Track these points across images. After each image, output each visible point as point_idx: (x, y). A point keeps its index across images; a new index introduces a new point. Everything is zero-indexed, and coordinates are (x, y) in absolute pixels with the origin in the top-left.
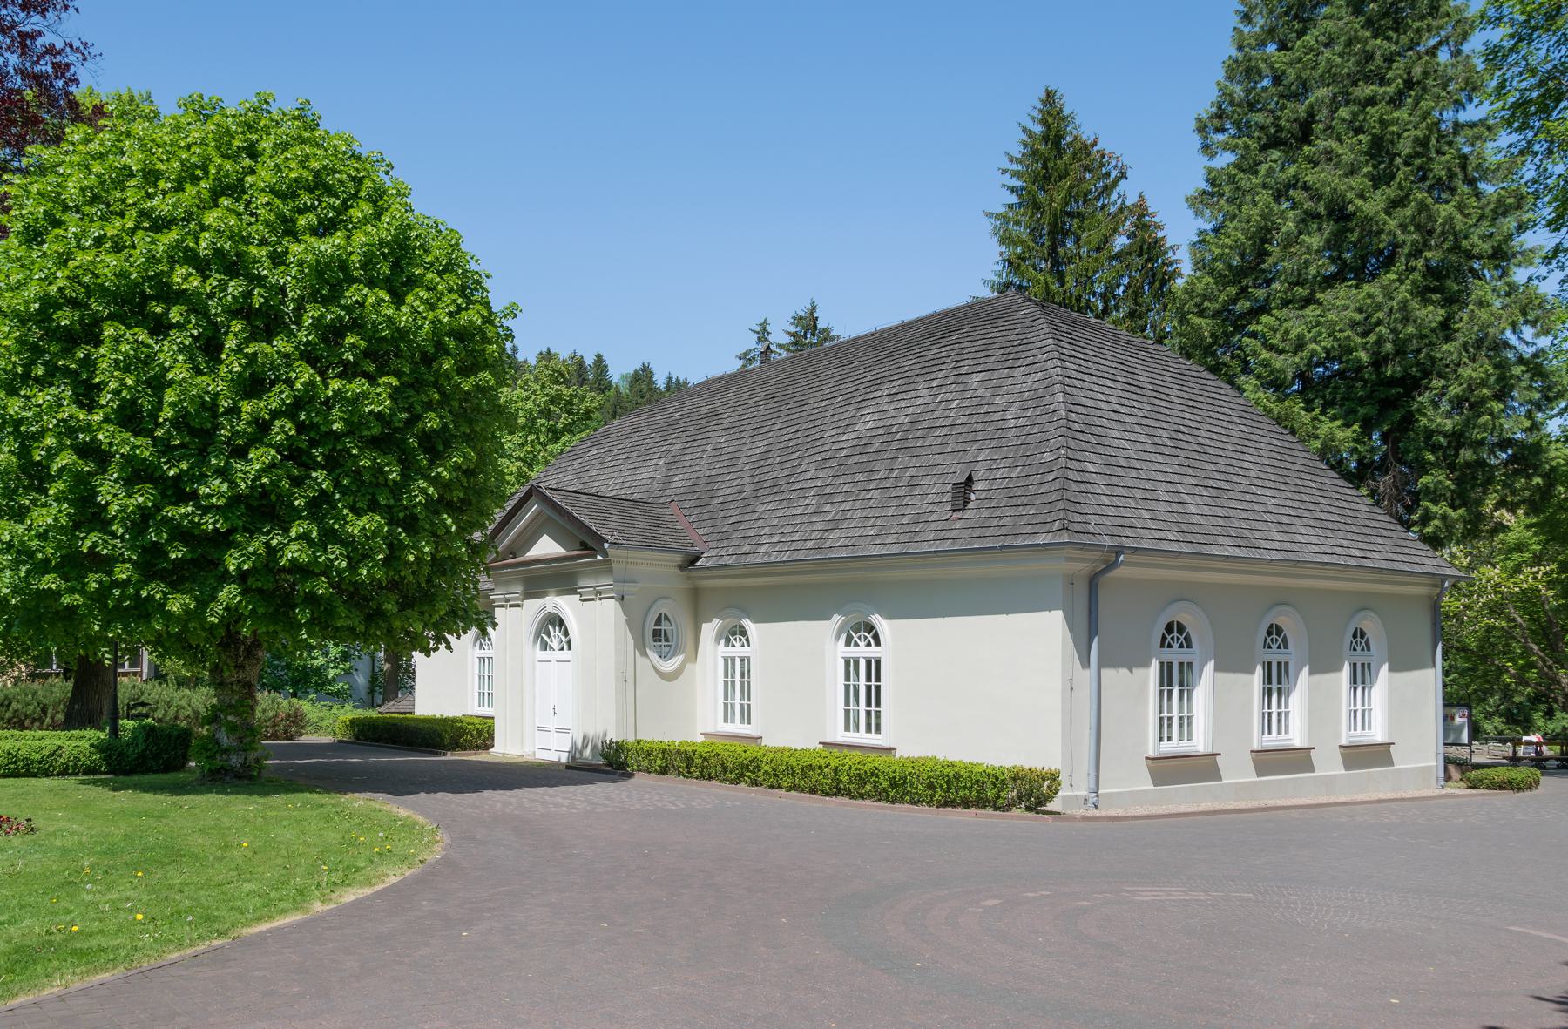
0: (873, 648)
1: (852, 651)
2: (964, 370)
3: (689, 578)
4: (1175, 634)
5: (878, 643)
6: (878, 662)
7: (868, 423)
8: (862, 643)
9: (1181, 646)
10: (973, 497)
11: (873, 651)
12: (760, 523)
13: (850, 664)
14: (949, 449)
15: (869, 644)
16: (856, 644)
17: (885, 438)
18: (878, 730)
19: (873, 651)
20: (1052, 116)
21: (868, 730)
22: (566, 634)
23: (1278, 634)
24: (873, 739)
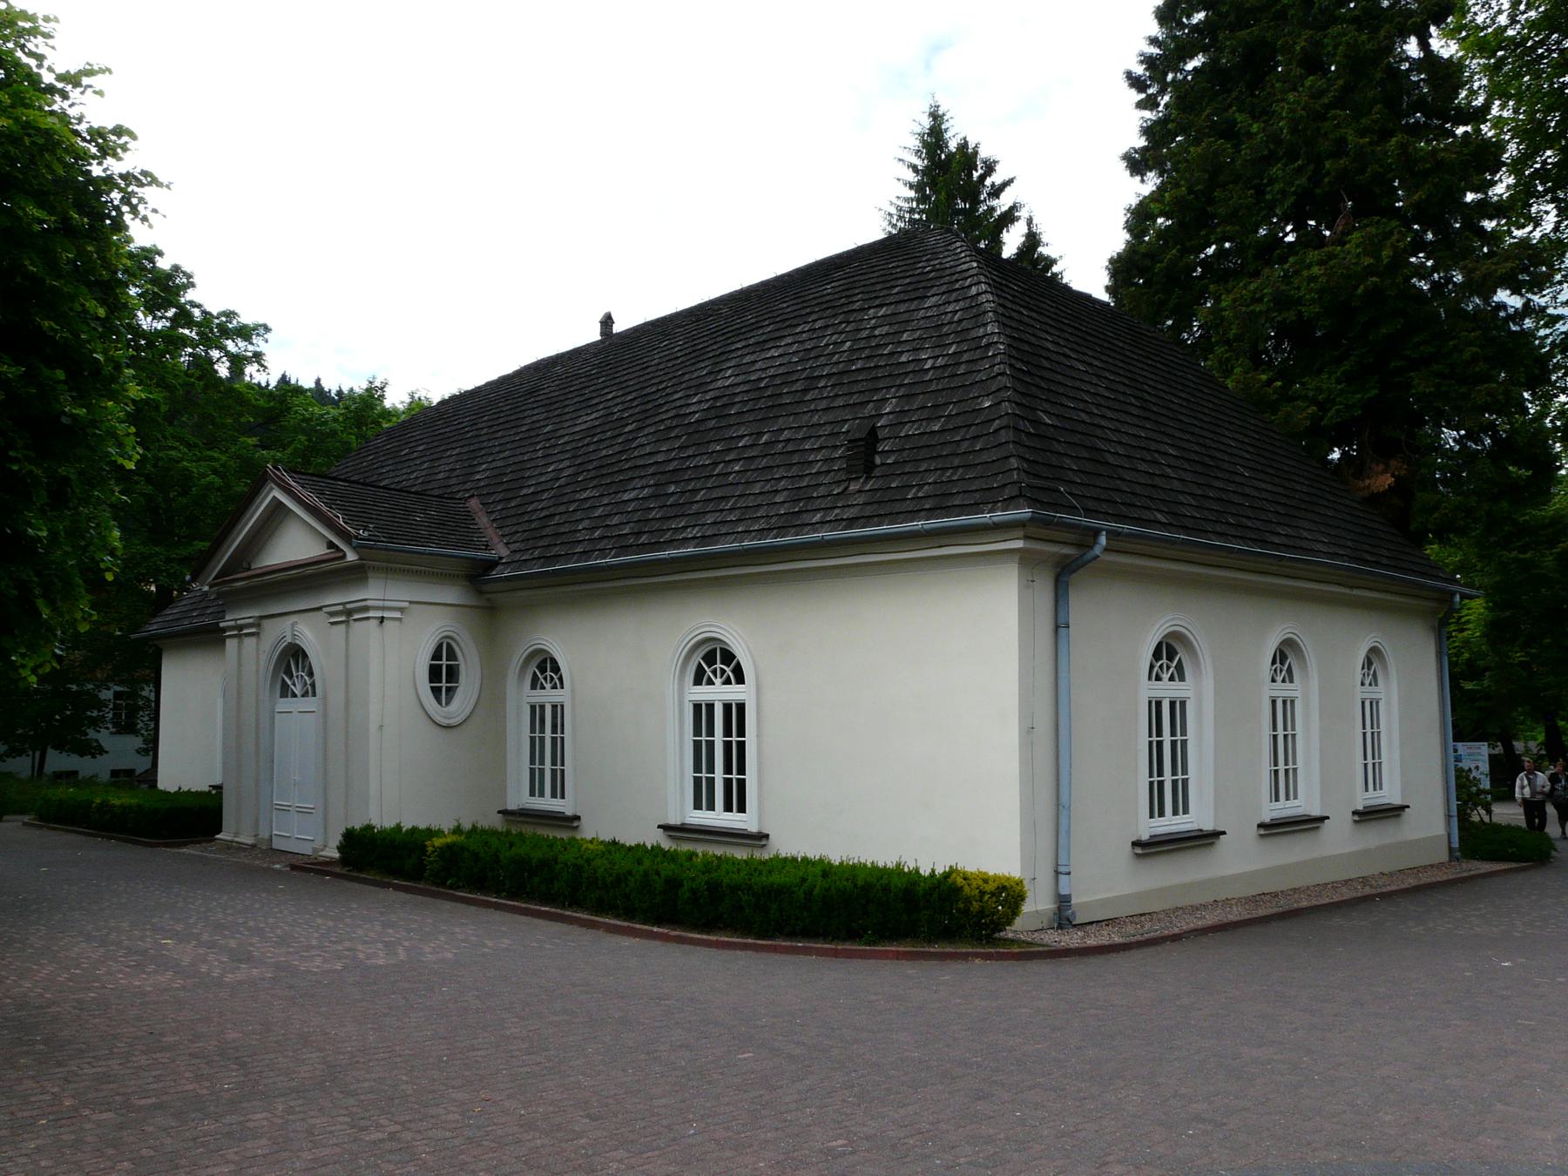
0: (735, 687)
1: (703, 693)
2: (856, 306)
3: (481, 593)
4: (719, 665)
5: (740, 679)
6: (741, 707)
7: (727, 379)
8: (718, 681)
9: (1171, 679)
10: (878, 460)
11: (734, 693)
12: (578, 516)
13: (703, 713)
14: (840, 402)
15: (728, 682)
16: (710, 682)
17: (751, 396)
18: (742, 809)
19: (734, 693)
20: (934, 138)
21: (728, 808)
22: (311, 674)
23: (1170, 658)
24: (733, 820)
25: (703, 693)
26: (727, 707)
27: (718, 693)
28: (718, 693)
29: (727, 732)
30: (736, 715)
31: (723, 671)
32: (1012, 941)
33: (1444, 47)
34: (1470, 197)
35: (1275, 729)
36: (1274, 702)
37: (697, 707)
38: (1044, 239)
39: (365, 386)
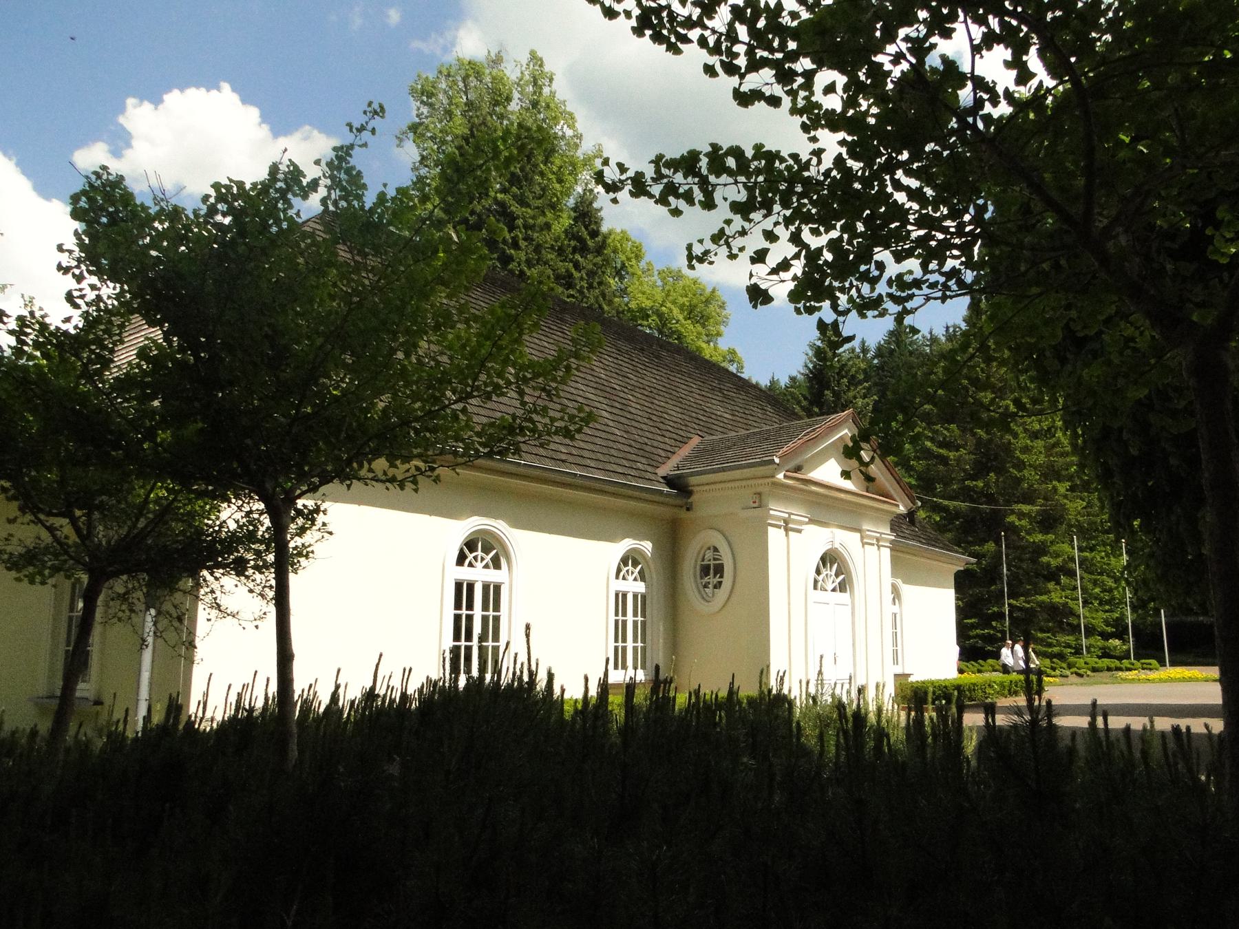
4: (479, 553)
6: (497, 588)
9: (635, 579)
11: (492, 576)
19: (492, 576)
25: (465, 574)
26: (486, 587)
27: (479, 574)
28: (479, 574)
29: (485, 607)
30: (493, 594)
31: (482, 559)
32: (821, 737)
33: (1169, 267)
34: (878, 34)
35: (1197, 680)
36: (617, 595)
37: (459, 586)
38: (669, 54)
39: (262, 175)
